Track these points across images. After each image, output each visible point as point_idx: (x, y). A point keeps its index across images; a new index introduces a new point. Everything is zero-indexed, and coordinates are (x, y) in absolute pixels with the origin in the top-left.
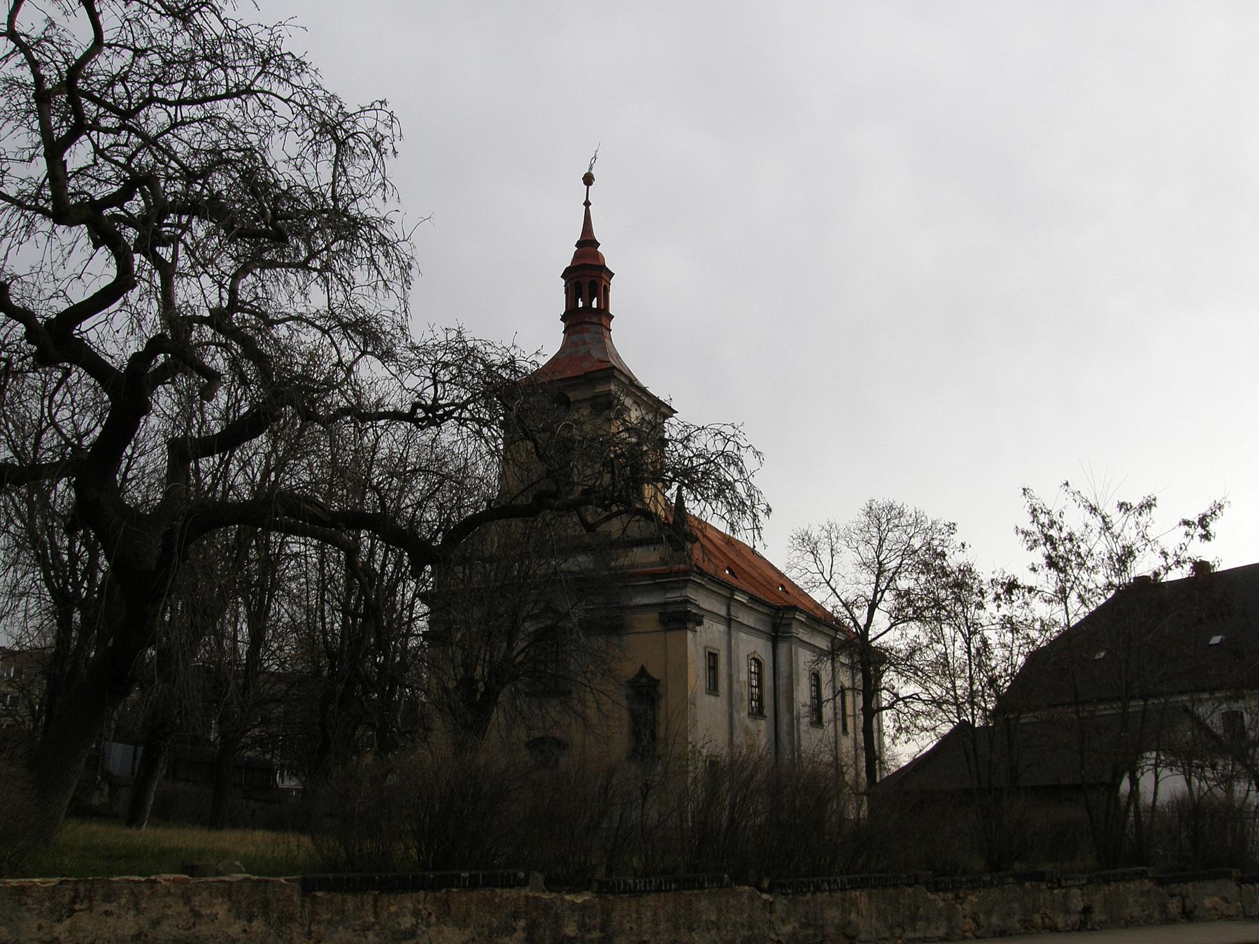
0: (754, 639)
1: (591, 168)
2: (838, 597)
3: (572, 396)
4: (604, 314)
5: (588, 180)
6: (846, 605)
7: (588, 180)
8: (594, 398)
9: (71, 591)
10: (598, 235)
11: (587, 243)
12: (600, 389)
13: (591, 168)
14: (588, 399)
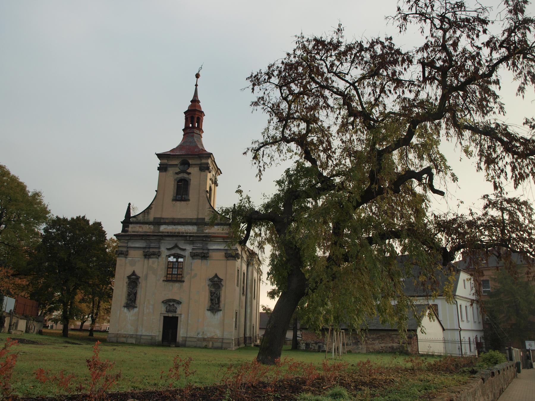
0: (183, 217)
1: (199, 71)
2: (350, 70)
3: (191, 162)
4: (200, 129)
5: (197, 76)
6: (353, 84)
7: (197, 76)
8: (201, 164)
9: (409, 124)
10: (200, 98)
11: (195, 101)
12: (204, 161)
13: (199, 71)
14: (198, 164)
